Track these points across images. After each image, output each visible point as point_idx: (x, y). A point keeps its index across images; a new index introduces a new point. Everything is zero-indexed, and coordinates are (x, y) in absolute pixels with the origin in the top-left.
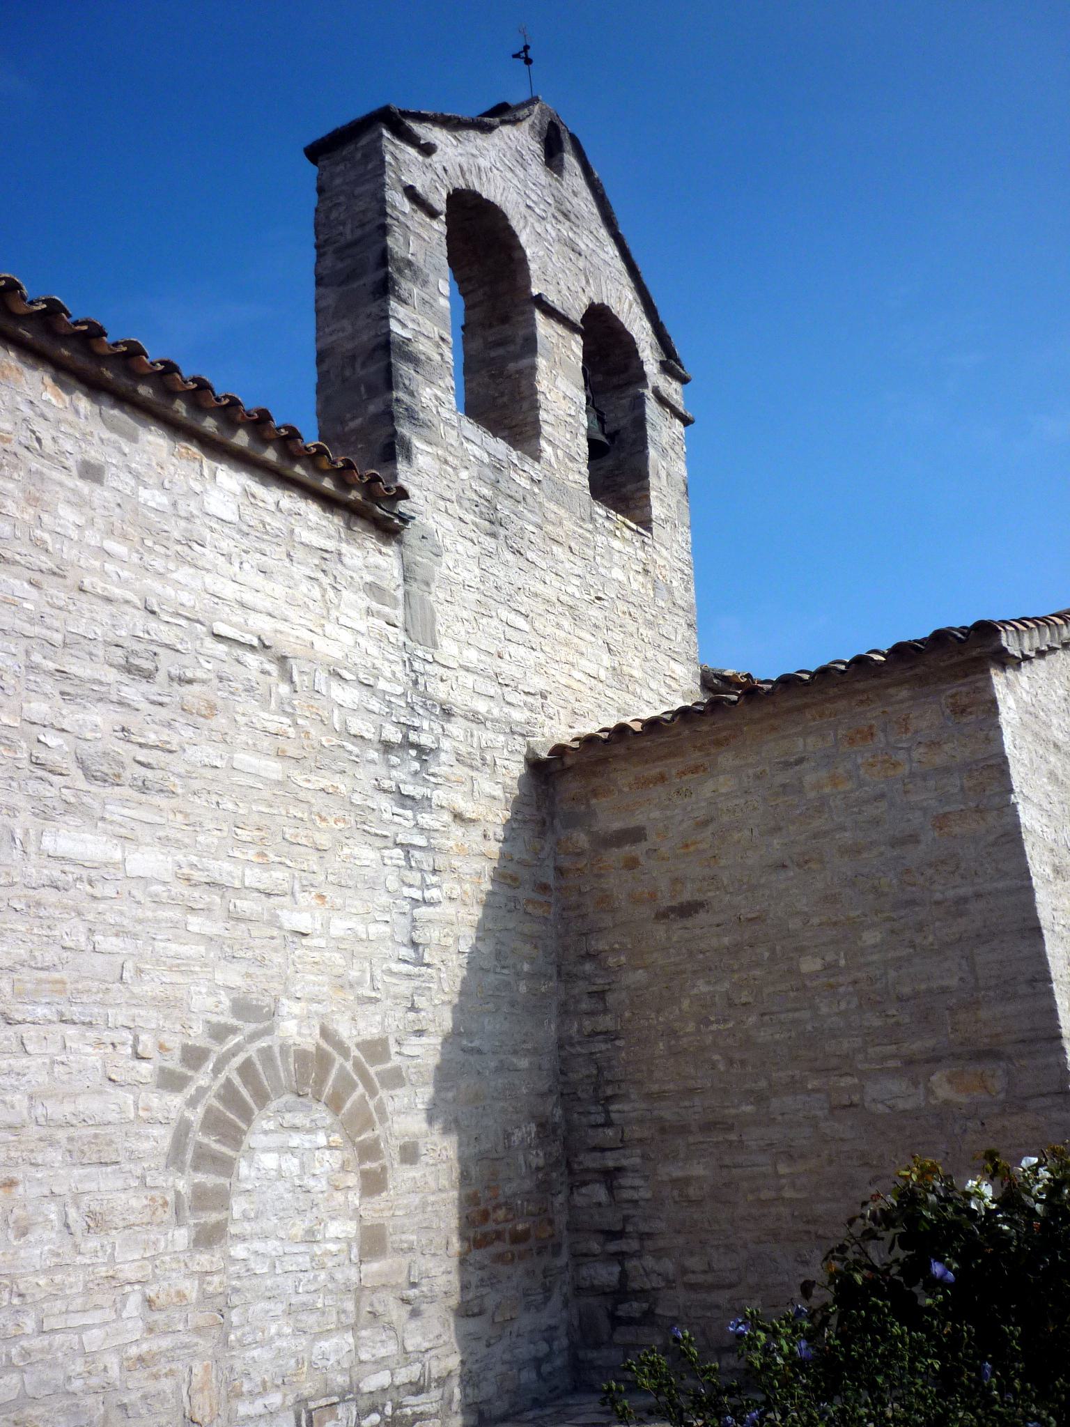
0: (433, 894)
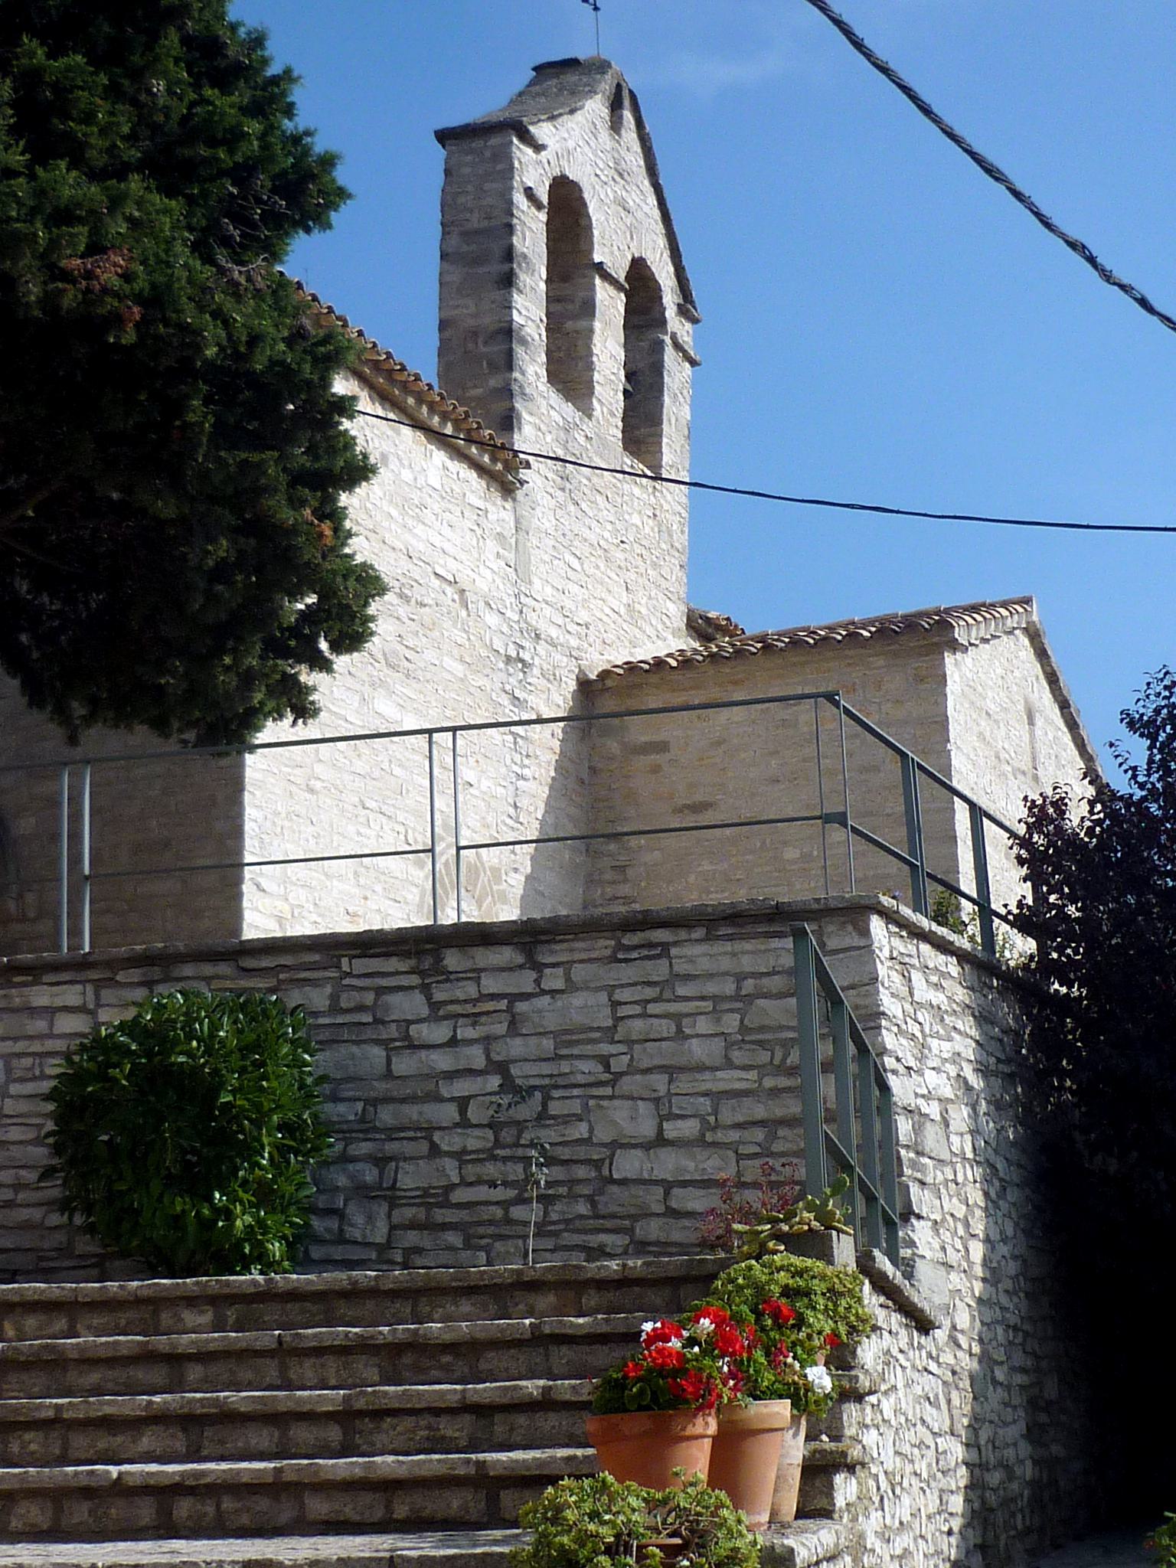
0: (526, 772)
